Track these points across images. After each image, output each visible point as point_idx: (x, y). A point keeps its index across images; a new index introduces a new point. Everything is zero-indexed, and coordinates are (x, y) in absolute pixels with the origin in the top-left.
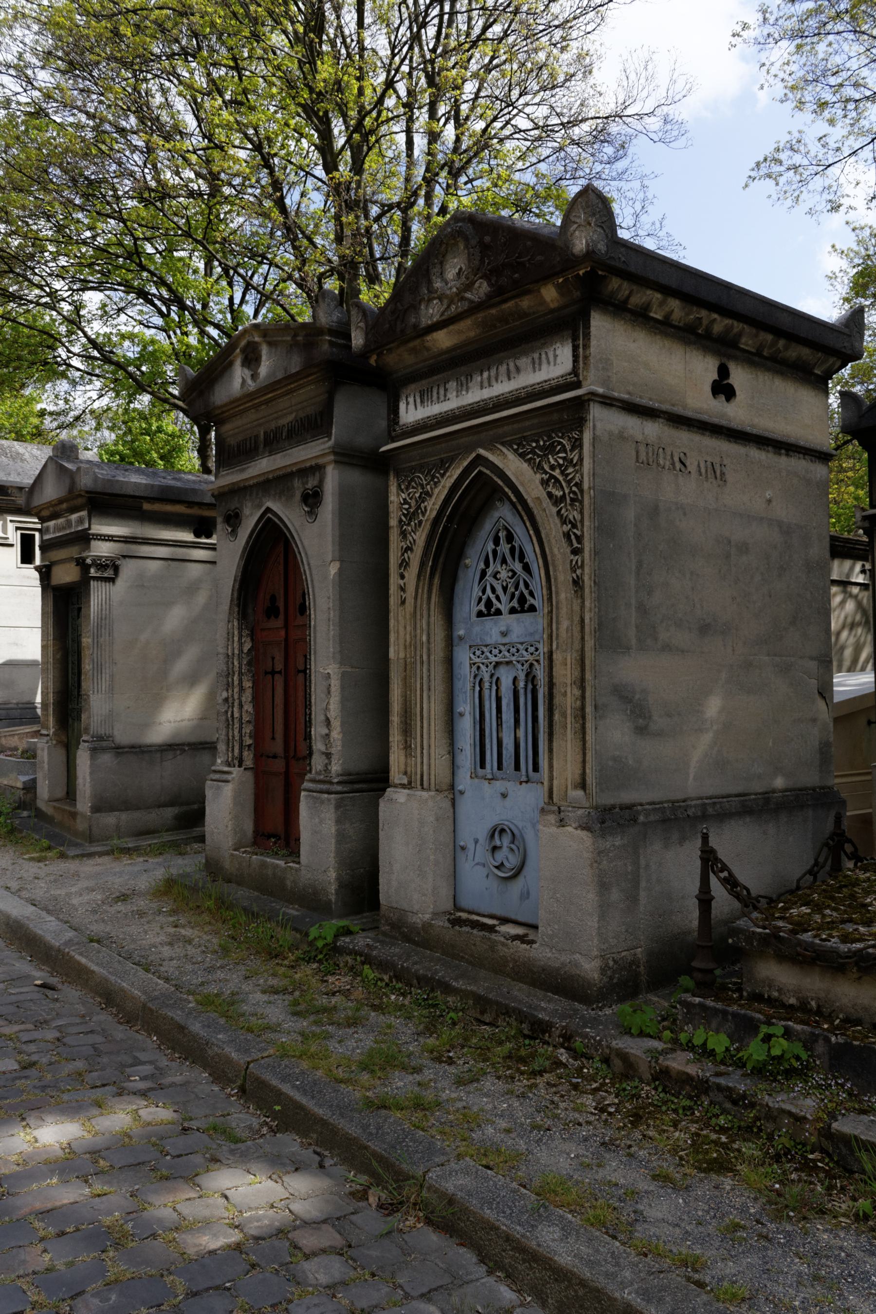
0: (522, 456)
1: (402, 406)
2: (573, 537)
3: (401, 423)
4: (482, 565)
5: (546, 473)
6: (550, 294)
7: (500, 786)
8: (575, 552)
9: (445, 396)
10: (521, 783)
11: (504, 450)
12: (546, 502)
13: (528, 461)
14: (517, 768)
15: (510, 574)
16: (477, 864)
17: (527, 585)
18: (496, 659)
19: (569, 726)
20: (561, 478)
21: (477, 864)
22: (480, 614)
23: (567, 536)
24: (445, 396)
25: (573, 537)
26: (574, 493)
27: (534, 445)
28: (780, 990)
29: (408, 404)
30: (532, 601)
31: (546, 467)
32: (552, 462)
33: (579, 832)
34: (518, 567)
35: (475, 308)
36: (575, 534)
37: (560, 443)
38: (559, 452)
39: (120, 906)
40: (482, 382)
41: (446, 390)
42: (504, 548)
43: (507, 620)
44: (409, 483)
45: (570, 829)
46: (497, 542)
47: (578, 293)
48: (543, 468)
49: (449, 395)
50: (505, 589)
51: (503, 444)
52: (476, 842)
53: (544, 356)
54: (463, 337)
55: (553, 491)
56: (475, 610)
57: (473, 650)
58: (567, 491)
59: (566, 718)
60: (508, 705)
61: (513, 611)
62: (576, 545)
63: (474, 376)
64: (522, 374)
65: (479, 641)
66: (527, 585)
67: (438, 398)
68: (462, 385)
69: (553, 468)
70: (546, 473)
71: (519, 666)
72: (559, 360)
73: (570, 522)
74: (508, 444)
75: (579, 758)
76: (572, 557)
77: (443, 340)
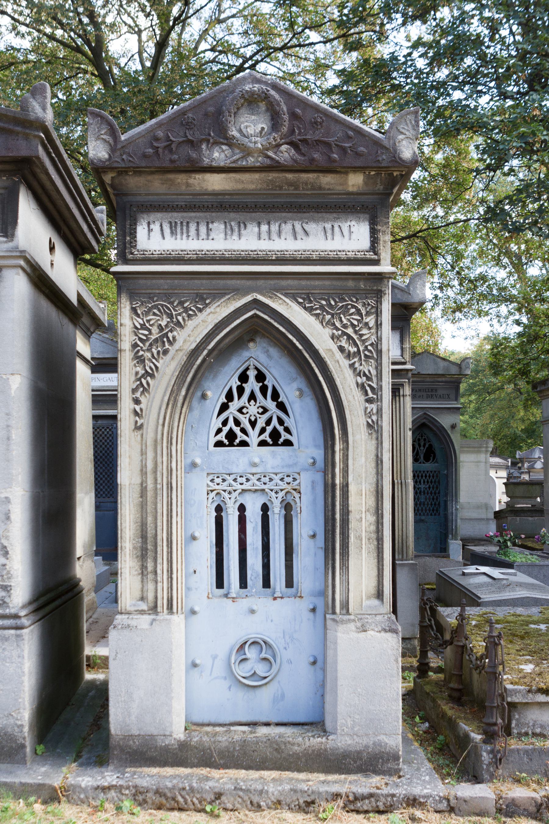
0: (310, 310)
1: (141, 231)
2: (368, 388)
3: (139, 247)
4: (223, 399)
5: (337, 329)
6: (355, 181)
7: (244, 604)
8: (369, 401)
9: (208, 235)
10: (275, 599)
11: (287, 300)
12: (338, 355)
13: (317, 315)
14: (266, 583)
15: (261, 410)
16: (216, 678)
17: (281, 422)
18: (243, 487)
19: (364, 546)
20: (355, 337)
21: (216, 678)
22: (219, 444)
23: (362, 387)
24: (208, 235)
25: (368, 388)
26: (370, 351)
27: (324, 302)
28: (542, 726)
29: (150, 230)
30: (288, 437)
31: (338, 324)
32: (345, 321)
33: (383, 634)
34: (271, 405)
35: (275, 167)
36: (369, 386)
37: (353, 307)
38: (352, 314)
39: (249, 802)
40: (259, 234)
41: (209, 230)
42: (252, 385)
43: (255, 452)
44: (150, 309)
45: (371, 633)
46: (243, 378)
47: (382, 187)
48: (334, 324)
49: (212, 235)
50: (253, 424)
51: (286, 295)
52: (215, 657)
53: (336, 229)
54: (240, 186)
55: (346, 346)
56: (213, 440)
57: (211, 477)
58: (361, 349)
59: (361, 540)
60: (254, 529)
61: (263, 443)
62: (370, 395)
63: (249, 226)
64: (311, 237)
65: (221, 470)
66: (281, 422)
67: (198, 235)
68: (232, 230)
69: (345, 326)
70: (337, 329)
71: (273, 494)
72: (353, 236)
73: (365, 375)
74: (294, 297)
75: (375, 573)
76: (367, 405)
77: (215, 183)
